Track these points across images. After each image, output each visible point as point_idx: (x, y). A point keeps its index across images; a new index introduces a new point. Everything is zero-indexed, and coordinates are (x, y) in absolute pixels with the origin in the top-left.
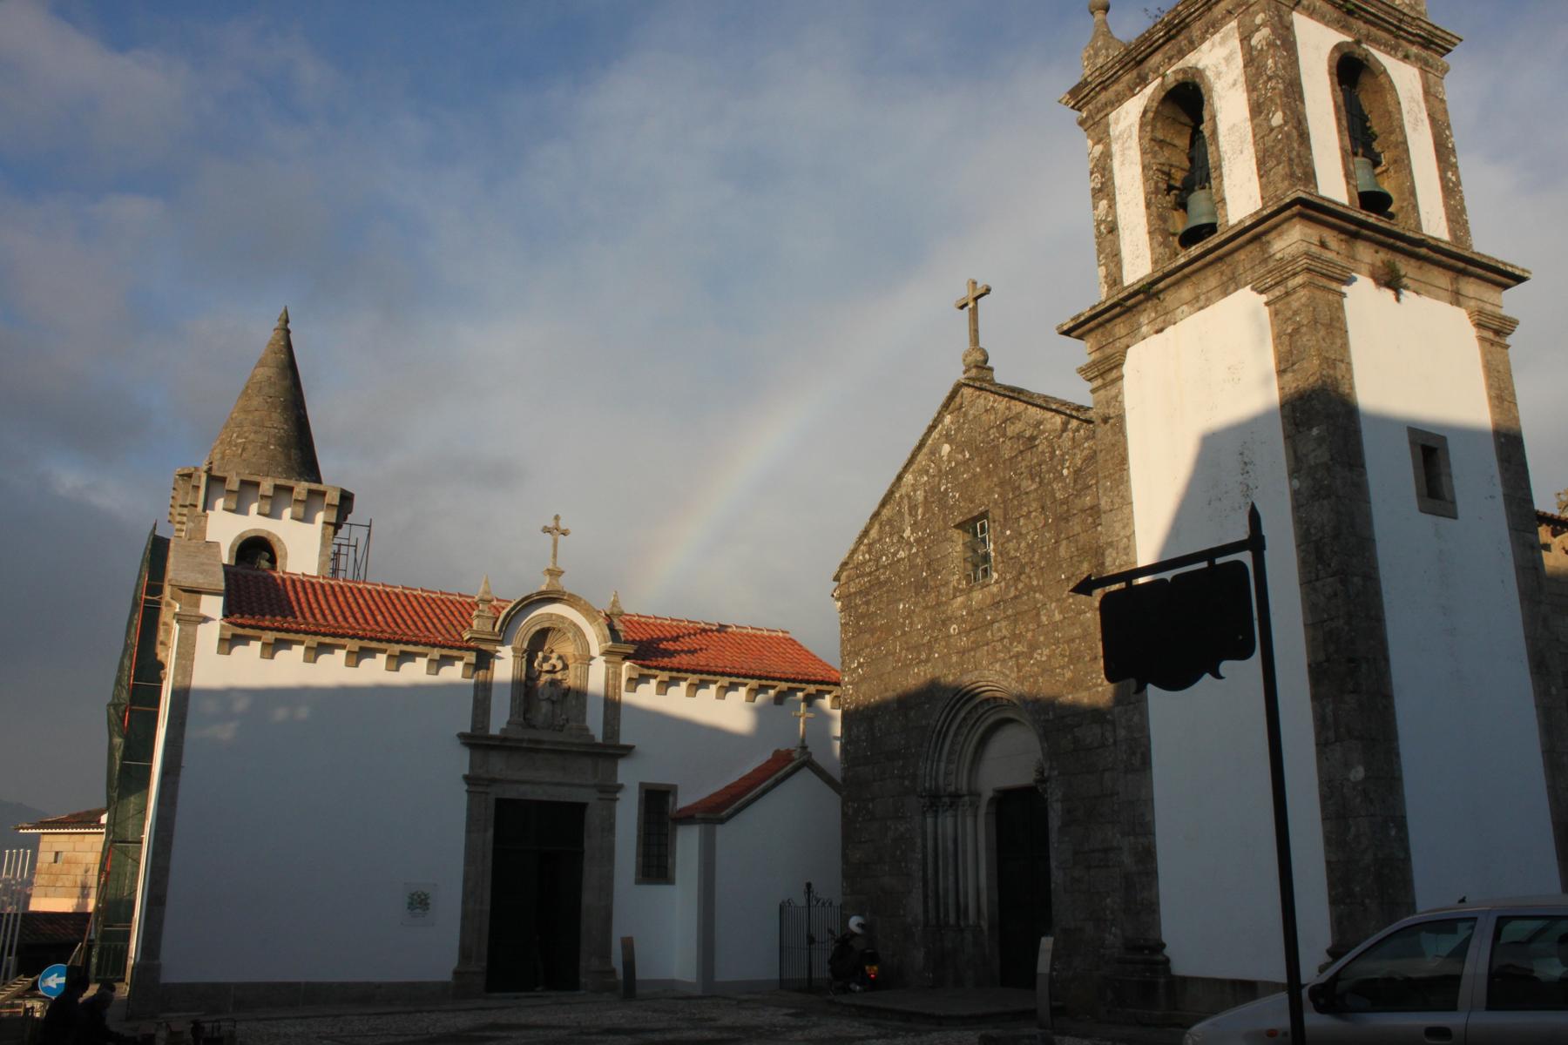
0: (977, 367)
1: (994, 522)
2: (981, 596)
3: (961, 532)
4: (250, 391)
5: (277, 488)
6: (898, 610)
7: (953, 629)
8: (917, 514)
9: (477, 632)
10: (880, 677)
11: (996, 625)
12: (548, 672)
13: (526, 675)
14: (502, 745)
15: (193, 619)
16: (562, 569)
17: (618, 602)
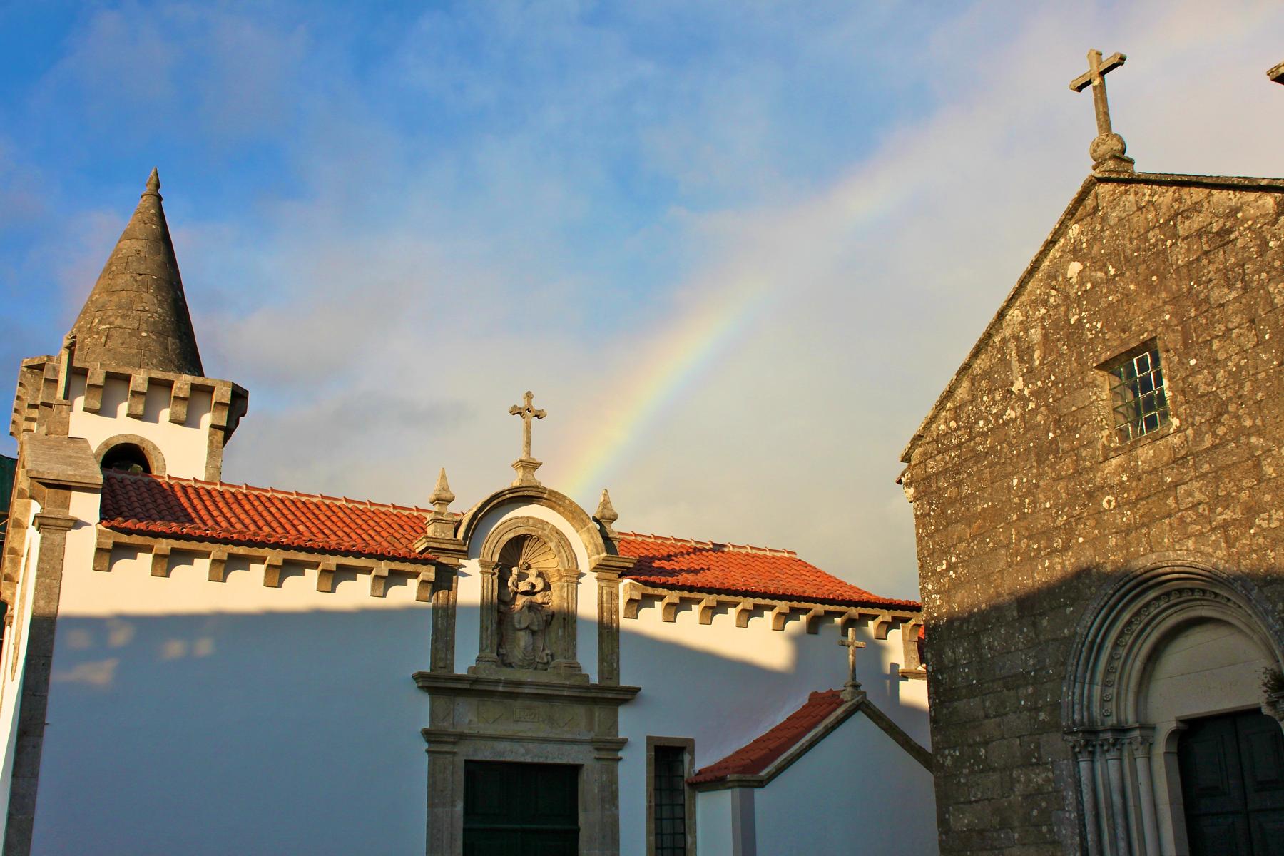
0: (1114, 157)
1: (1168, 351)
2: (1151, 452)
3: (1106, 373)
4: (114, 268)
5: (152, 382)
6: (1010, 488)
7: (1107, 502)
8: (1031, 358)
9: (435, 539)
10: (987, 578)
11: (1182, 490)
12: (525, 593)
13: (498, 599)
14: (472, 689)
15: (60, 523)
16: (539, 460)
17: (610, 502)
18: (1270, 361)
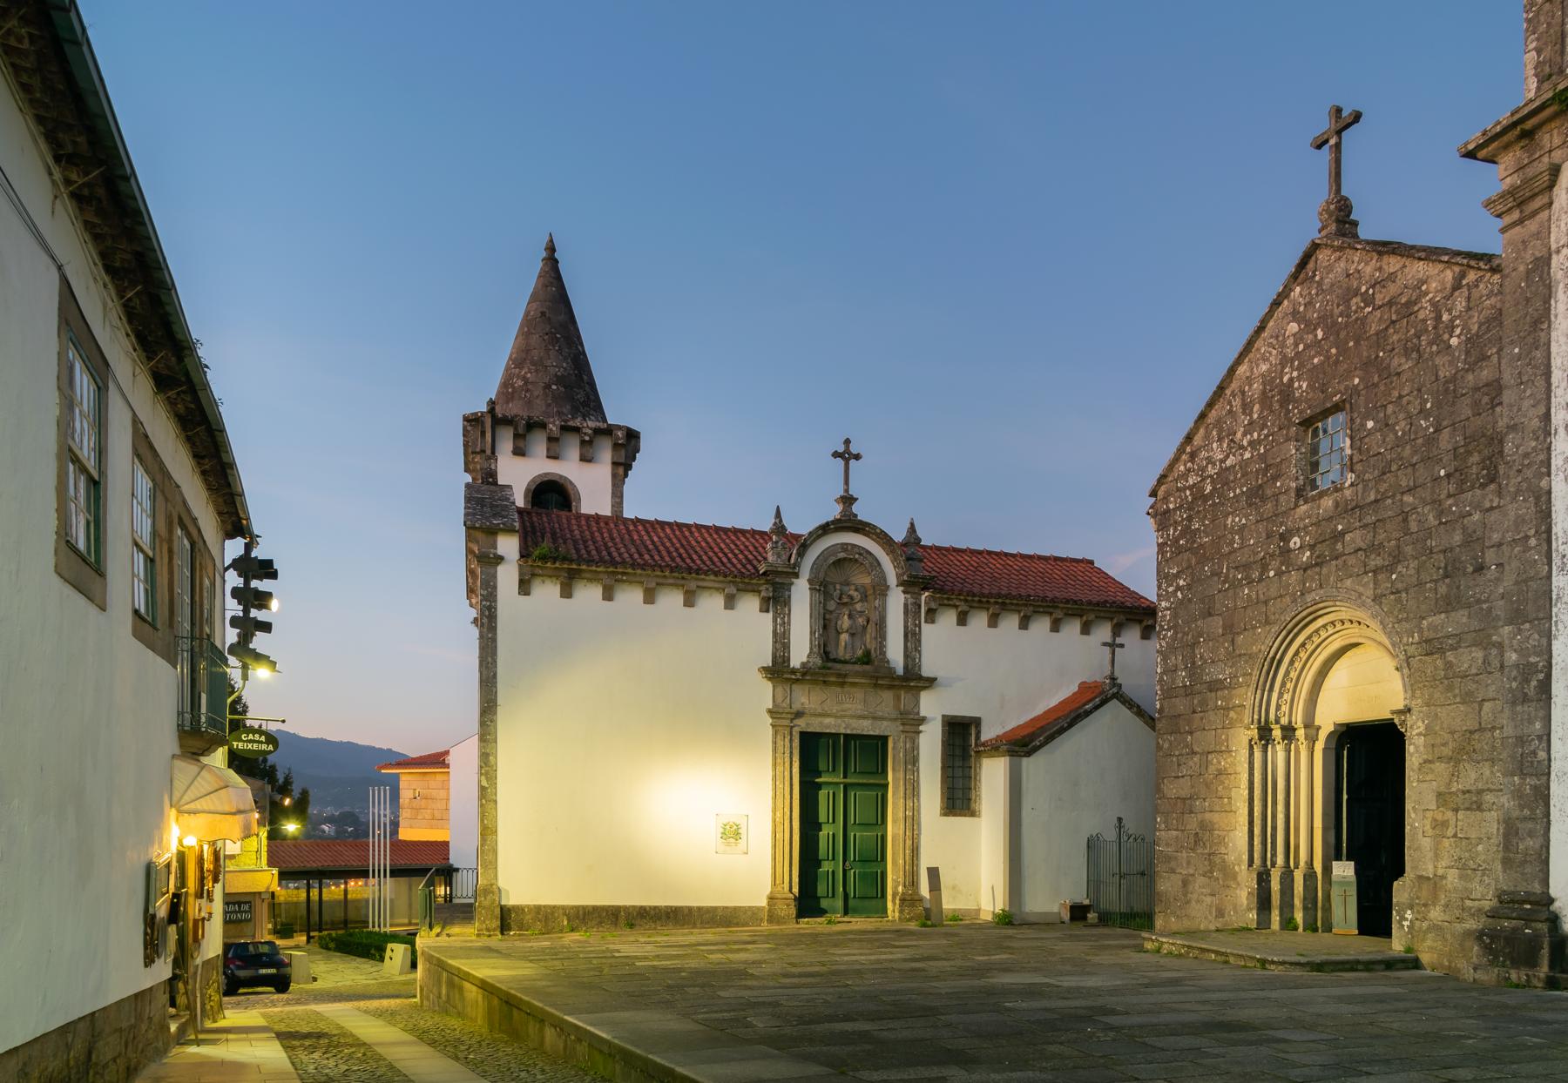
18: (1427, 428)
